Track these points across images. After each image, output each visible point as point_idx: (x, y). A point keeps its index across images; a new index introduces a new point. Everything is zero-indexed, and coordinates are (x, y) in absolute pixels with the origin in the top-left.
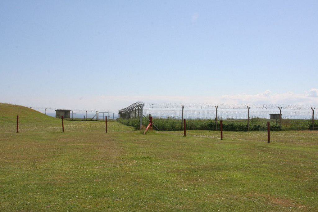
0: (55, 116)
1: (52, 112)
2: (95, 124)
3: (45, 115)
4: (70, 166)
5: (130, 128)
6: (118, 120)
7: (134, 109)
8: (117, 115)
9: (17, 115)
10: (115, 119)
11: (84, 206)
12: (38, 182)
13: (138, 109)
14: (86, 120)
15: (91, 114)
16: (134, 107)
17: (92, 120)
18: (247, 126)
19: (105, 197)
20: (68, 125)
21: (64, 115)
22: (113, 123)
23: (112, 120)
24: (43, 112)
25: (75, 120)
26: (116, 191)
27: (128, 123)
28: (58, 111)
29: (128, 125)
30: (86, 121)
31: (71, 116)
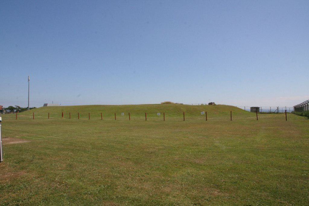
0: (250, 111)
1: (248, 109)
2: (276, 115)
3: (245, 111)
4: (266, 140)
5: (303, 118)
6: (293, 113)
7: (306, 105)
8: (292, 109)
9: (208, 121)
10: (291, 111)
11: (280, 163)
12: (249, 147)
13: (304, 106)
14: (270, 113)
15: (274, 108)
16: (306, 104)
17: (274, 113)
18: (28, 108)
19: (294, 159)
20: (260, 116)
21: (256, 110)
22: (283, 114)
23: (289, 113)
24: (243, 108)
25: (263, 113)
26: (301, 157)
27: (302, 114)
28: (252, 108)
29: (302, 115)
30: (270, 113)
31: (260, 111)
